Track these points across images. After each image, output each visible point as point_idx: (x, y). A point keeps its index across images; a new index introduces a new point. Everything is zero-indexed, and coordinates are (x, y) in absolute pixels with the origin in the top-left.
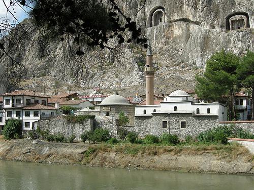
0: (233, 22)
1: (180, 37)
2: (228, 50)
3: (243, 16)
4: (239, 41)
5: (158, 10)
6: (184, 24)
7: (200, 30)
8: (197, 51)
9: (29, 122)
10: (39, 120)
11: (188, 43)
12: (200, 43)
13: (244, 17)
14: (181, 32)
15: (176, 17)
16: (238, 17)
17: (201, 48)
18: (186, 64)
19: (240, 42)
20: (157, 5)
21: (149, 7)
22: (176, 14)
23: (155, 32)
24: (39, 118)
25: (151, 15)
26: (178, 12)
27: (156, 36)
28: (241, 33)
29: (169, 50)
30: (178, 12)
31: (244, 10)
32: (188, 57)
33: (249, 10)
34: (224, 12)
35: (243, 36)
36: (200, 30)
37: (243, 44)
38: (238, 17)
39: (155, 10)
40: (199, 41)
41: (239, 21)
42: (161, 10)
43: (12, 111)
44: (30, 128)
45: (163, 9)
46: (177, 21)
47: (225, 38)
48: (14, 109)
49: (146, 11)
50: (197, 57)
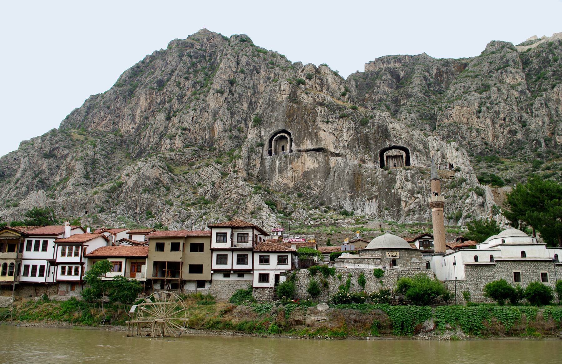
0: (388, 157)
1: (314, 171)
2: (393, 191)
3: (401, 151)
4: (407, 180)
5: (278, 135)
6: (321, 156)
7: (346, 164)
8: (344, 191)
9: (268, 275)
10: (289, 271)
11: (330, 180)
12: (348, 181)
13: (403, 153)
14: (316, 165)
15: (308, 145)
16: (394, 152)
17: (350, 188)
18: (328, 208)
19: (410, 183)
20: (280, 128)
21: (268, 129)
22: (308, 142)
23: (278, 163)
24: (288, 267)
25: (271, 140)
26: (312, 140)
27: (280, 168)
28: (409, 171)
29: (298, 188)
30: (312, 140)
31: (401, 144)
32: (330, 198)
33: (410, 145)
34: (376, 145)
35: (413, 175)
36: (346, 164)
37: (414, 185)
38: (394, 152)
39: (276, 134)
40: (347, 178)
41: (396, 157)
42: (286, 135)
43: (229, 254)
44: (271, 283)
45: (289, 134)
46: (310, 150)
47: (385, 177)
48: (232, 250)
49: (263, 133)
50: (345, 199)
